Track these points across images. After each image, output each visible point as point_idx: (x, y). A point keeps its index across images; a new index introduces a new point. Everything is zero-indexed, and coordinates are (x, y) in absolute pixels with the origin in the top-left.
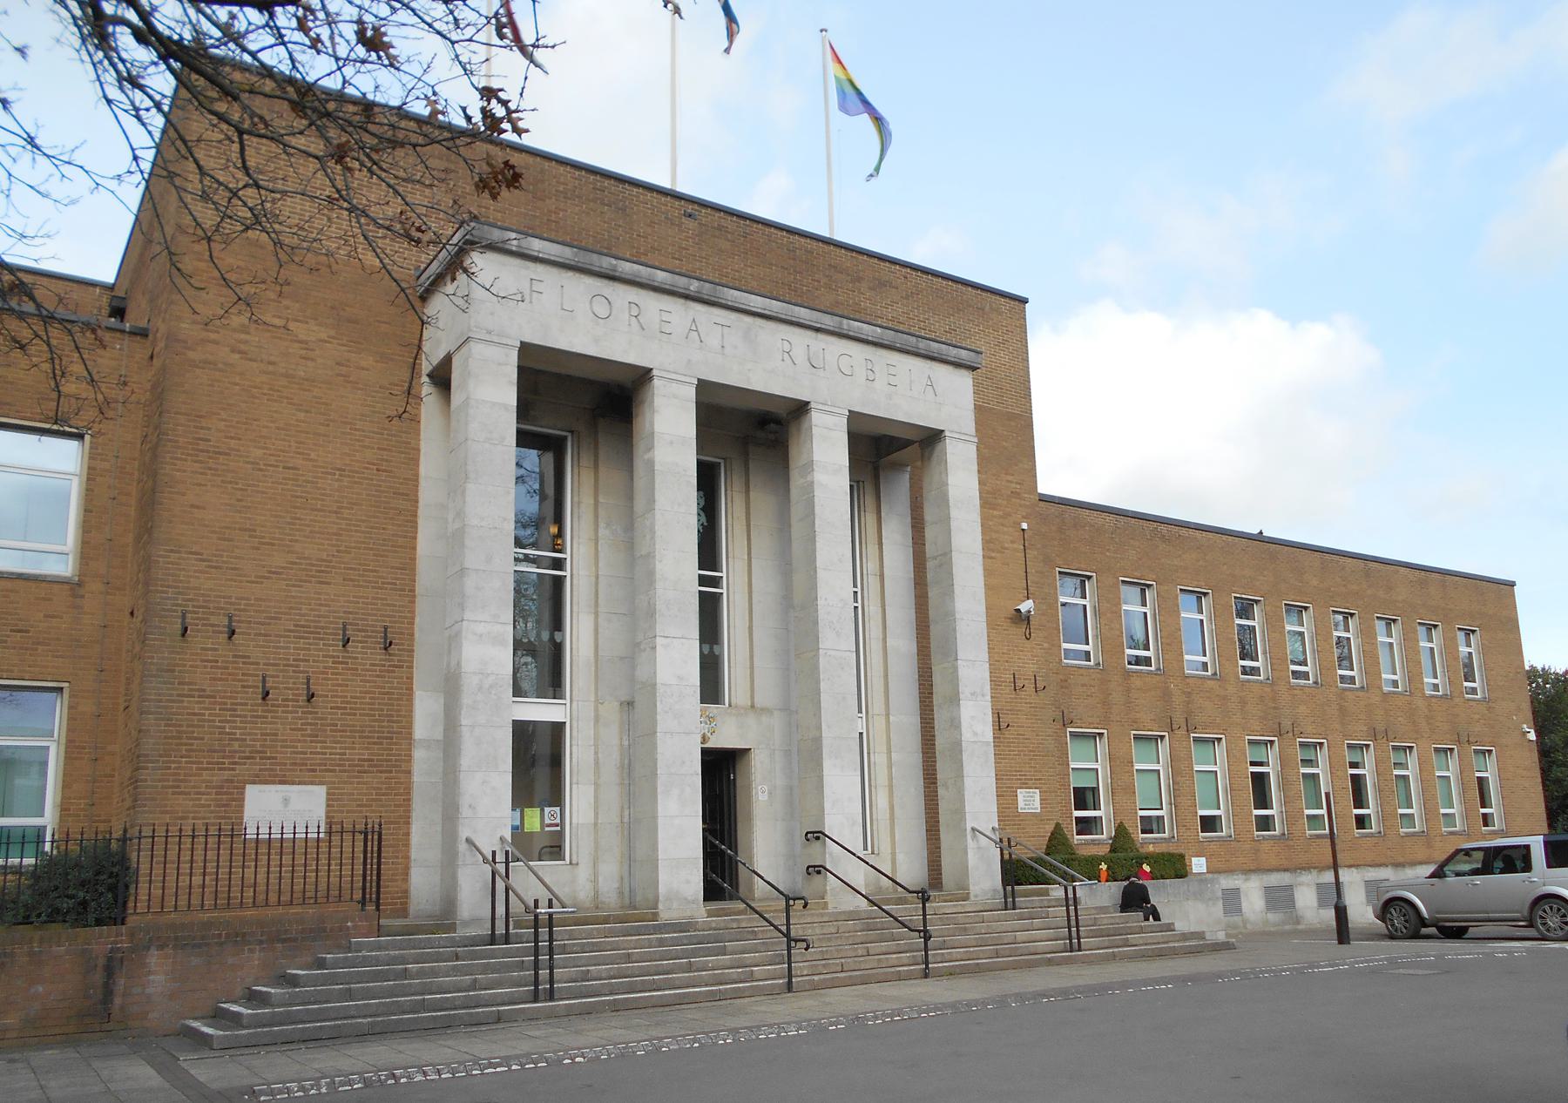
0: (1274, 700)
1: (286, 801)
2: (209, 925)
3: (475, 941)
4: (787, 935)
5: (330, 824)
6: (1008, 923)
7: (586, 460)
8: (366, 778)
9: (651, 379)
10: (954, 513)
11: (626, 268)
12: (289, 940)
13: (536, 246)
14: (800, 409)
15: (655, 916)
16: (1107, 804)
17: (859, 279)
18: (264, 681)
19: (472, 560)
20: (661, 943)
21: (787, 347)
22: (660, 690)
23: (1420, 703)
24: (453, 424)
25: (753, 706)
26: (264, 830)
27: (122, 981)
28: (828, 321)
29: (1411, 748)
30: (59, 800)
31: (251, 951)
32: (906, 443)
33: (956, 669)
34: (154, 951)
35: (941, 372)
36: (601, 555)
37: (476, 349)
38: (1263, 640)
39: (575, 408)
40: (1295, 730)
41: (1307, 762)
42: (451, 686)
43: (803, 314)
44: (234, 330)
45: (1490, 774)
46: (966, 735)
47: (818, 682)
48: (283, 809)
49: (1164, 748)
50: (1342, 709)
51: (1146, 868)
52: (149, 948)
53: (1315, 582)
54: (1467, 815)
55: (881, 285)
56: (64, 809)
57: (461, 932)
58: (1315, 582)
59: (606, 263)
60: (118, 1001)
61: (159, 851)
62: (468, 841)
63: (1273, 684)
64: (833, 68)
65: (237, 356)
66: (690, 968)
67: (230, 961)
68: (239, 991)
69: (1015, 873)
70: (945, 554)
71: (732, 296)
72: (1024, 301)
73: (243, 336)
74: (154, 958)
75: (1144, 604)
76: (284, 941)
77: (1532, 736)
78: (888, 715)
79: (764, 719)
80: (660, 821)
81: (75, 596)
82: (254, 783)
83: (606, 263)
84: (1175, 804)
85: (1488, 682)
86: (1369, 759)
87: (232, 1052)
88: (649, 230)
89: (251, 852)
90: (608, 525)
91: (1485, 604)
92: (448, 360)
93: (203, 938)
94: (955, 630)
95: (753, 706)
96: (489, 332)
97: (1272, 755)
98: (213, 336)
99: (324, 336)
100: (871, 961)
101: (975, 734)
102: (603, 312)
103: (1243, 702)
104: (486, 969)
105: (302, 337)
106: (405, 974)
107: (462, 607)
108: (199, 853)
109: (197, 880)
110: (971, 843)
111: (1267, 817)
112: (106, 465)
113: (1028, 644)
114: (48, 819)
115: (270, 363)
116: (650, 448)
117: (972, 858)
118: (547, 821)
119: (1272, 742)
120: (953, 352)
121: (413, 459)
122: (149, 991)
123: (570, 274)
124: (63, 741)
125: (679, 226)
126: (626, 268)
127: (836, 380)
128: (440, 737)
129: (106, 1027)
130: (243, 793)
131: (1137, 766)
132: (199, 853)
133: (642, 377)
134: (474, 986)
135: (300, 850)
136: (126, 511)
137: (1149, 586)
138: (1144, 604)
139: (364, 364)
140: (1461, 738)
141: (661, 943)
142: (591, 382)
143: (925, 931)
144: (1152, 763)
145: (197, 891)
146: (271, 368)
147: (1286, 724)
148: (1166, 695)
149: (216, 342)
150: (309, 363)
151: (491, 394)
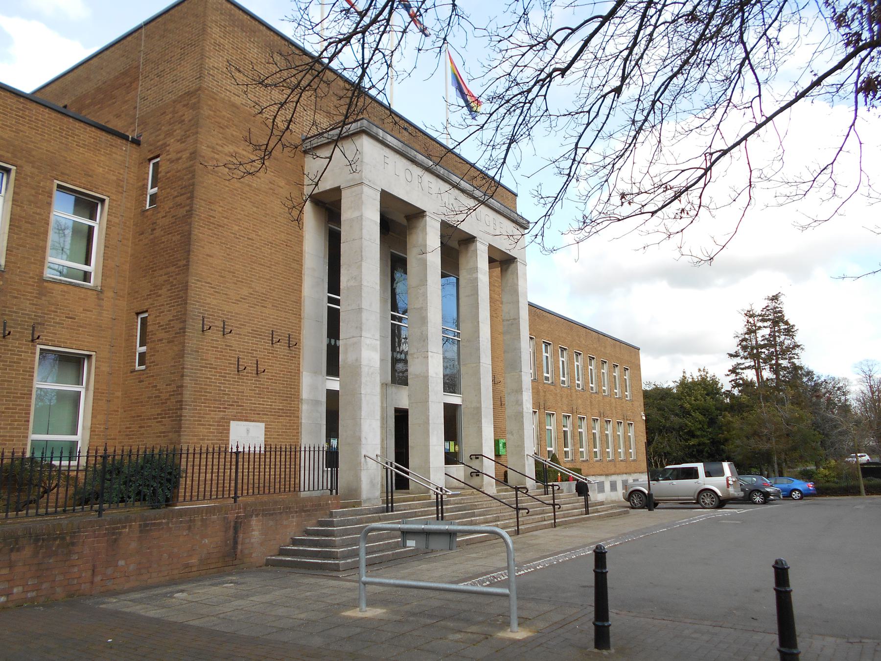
3: (370, 511)
8: (281, 419)
22: (430, 379)
23: (613, 400)
30: (89, 424)
31: (293, 517)
33: (520, 376)
34: (254, 518)
37: (366, 189)
44: (226, 154)
46: (525, 410)
48: (247, 435)
50: (591, 402)
57: (365, 506)
60: (239, 547)
61: (190, 459)
67: (285, 523)
68: (288, 540)
74: (254, 521)
76: (305, 511)
77: (644, 418)
80: (431, 447)
81: (99, 299)
82: (234, 420)
91: (625, 355)
93: (274, 510)
98: (216, 156)
103: (562, 397)
108: (210, 460)
109: (209, 476)
112: (117, 220)
114: (81, 438)
121: (300, 242)
122: (253, 540)
123: (398, 156)
129: (235, 562)
130: (229, 426)
132: (210, 460)
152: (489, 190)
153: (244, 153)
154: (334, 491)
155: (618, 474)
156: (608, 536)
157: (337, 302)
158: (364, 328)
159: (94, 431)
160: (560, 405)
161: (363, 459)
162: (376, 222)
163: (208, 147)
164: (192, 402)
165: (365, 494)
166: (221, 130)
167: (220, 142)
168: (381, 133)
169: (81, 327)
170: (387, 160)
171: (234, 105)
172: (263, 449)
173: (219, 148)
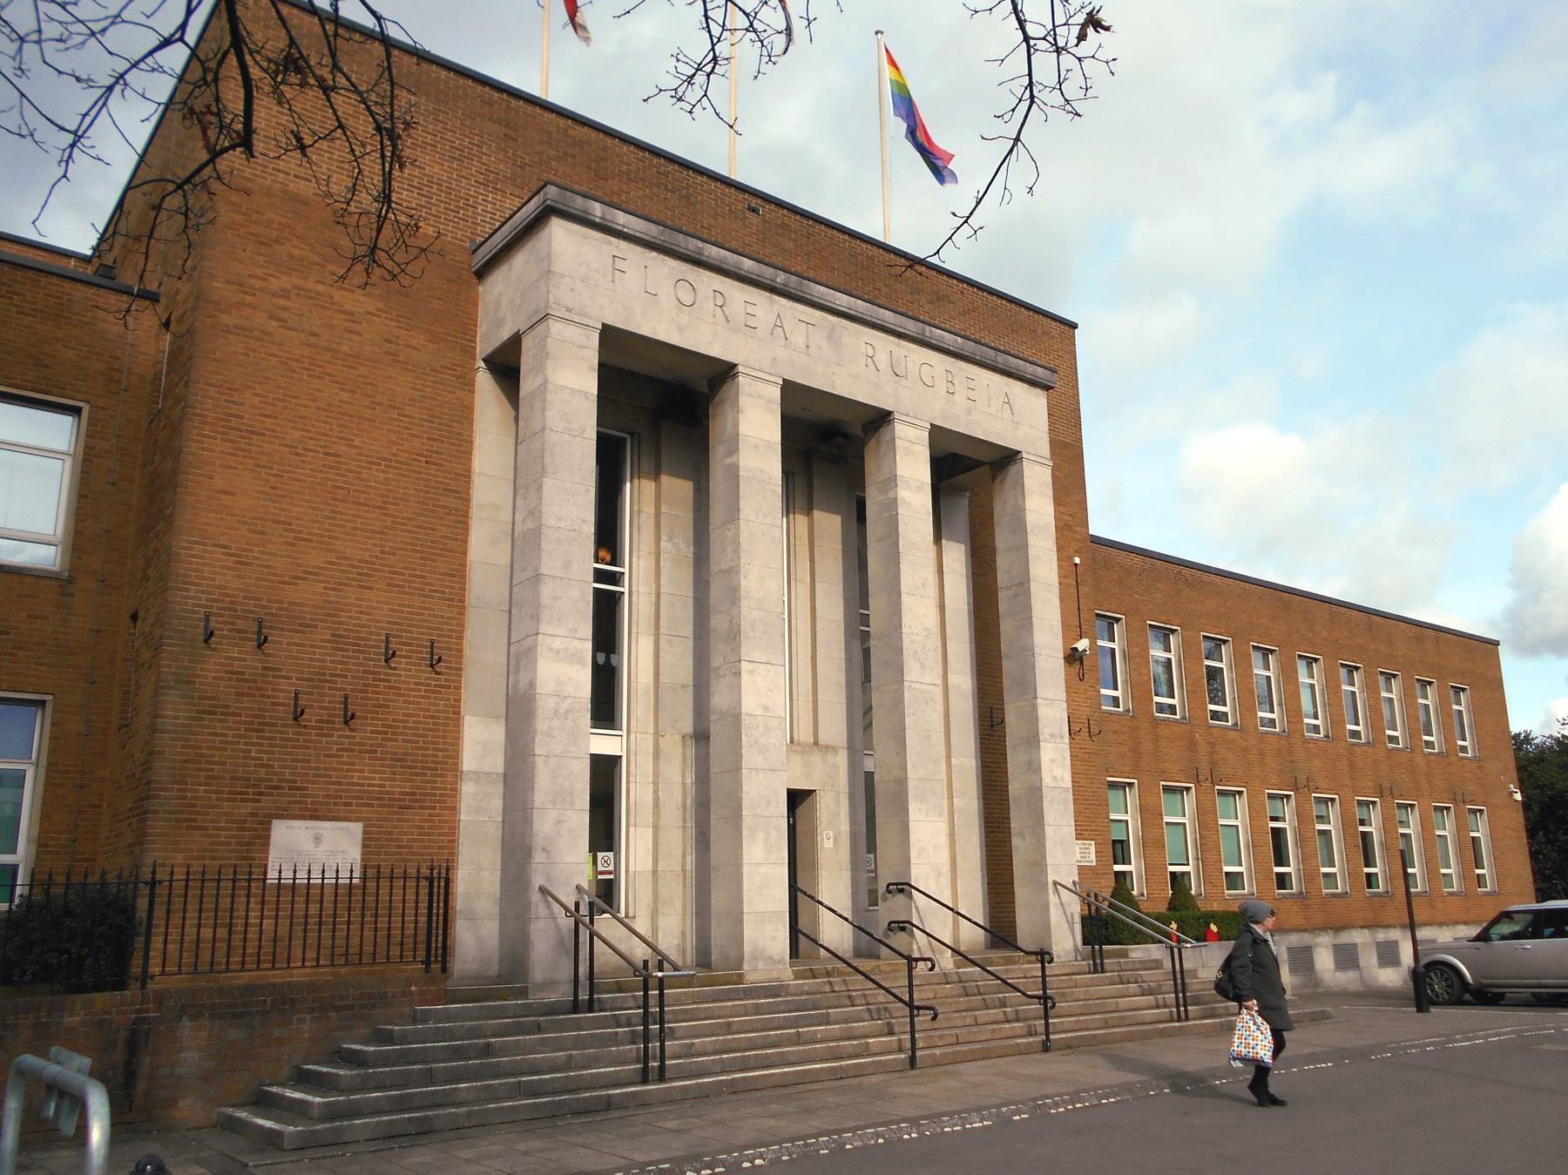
0: (1289, 752)
1: (317, 839)
2: (250, 989)
3: (553, 1009)
4: (910, 1004)
5: (365, 868)
6: (1102, 987)
7: (647, 465)
9: (735, 375)
10: (1031, 540)
11: (713, 252)
12: (345, 1007)
13: (622, 219)
14: (880, 419)
15: (740, 979)
16: (1490, 865)
17: (918, 292)
18: (296, 698)
19: (548, 565)
20: (757, 1010)
21: (870, 352)
23: (1419, 760)
24: (523, 411)
25: (816, 743)
26: (287, 874)
27: (148, 1061)
28: (911, 327)
29: (1412, 806)
30: (35, 833)
32: (978, 464)
33: (1035, 708)
34: (186, 1022)
35: (1018, 388)
36: (663, 571)
37: (556, 327)
38: (1279, 690)
39: (659, 407)
40: (1310, 786)
41: (1321, 819)
42: (519, 712)
43: (887, 316)
44: (274, 294)
45: (1481, 832)
46: (1047, 780)
47: (903, 717)
48: (316, 850)
49: (1190, 801)
50: (1352, 765)
51: (1214, 928)
52: (180, 1018)
53: (1324, 634)
54: (1352, 874)
55: (939, 299)
56: (42, 845)
57: (534, 998)
58: (1324, 634)
59: (693, 245)
60: (142, 1085)
62: (542, 890)
63: (1289, 736)
64: (887, 70)
65: (275, 324)
66: (798, 1040)
67: (277, 1033)
68: (285, 1072)
69: (1103, 929)
70: (1021, 584)
71: (819, 292)
72: (1074, 326)
73: (282, 302)
75: (1168, 650)
76: (337, 1009)
77: (1518, 797)
78: (949, 757)
79: (830, 757)
80: (746, 869)
82: (281, 817)
83: (693, 245)
84: (1202, 859)
85: (1479, 742)
86: (1375, 816)
87: (311, 1153)
88: (713, 222)
89: (271, 898)
90: (670, 539)
92: (515, 341)
94: (1034, 667)
95: (816, 743)
96: (569, 310)
97: (1289, 810)
98: (248, 299)
99: (372, 308)
100: (983, 1033)
101: (1055, 778)
102: (687, 300)
103: (1262, 755)
104: (579, 1043)
105: (347, 307)
106: (487, 1050)
107: (536, 618)
110: (1053, 898)
111: (1124, 873)
113: (1082, 686)
115: (313, 334)
116: (734, 450)
117: (1055, 915)
118: (600, 868)
119: (1288, 797)
120: (1030, 368)
121: (464, 449)
122: (179, 1071)
124: (43, 763)
125: (743, 220)
126: (713, 252)
127: (923, 392)
128: (501, 771)
130: (269, 830)
131: (1167, 819)
133: (722, 373)
134: (568, 1065)
135: (329, 893)
136: (127, 496)
137: (1173, 631)
138: (1168, 650)
139: (414, 342)
140: (1460, 800)
141: (757, 1010)
142: (650, 380)
143: (1044, 999)
144: (1181, 814)
145: (206, 947)
146: (313, 340)
147: (1302, 778)
148: (1192, 745)
149: (250, 306)
150: (354, 337)
151: (569, 385)
152: (1024, 338)
153: (321, 288)
154: (436, 967)
155: (1441, 924)
156: (1063, 1090)
157: (614, 578)
158: (545, 614)
159: (47, 846)
160: (1257, 771)
161: (536, 897)
162: (586, 395)
163: (228, 282)
164: (175, 782)
165: (538, 974)
166: (263, 249)
167: (260, 272)
168: (597, 210)
169: (21, 648)
170: (620, 264)
171: (297, 199)
172: (357, 874)
173: (258, 283)
